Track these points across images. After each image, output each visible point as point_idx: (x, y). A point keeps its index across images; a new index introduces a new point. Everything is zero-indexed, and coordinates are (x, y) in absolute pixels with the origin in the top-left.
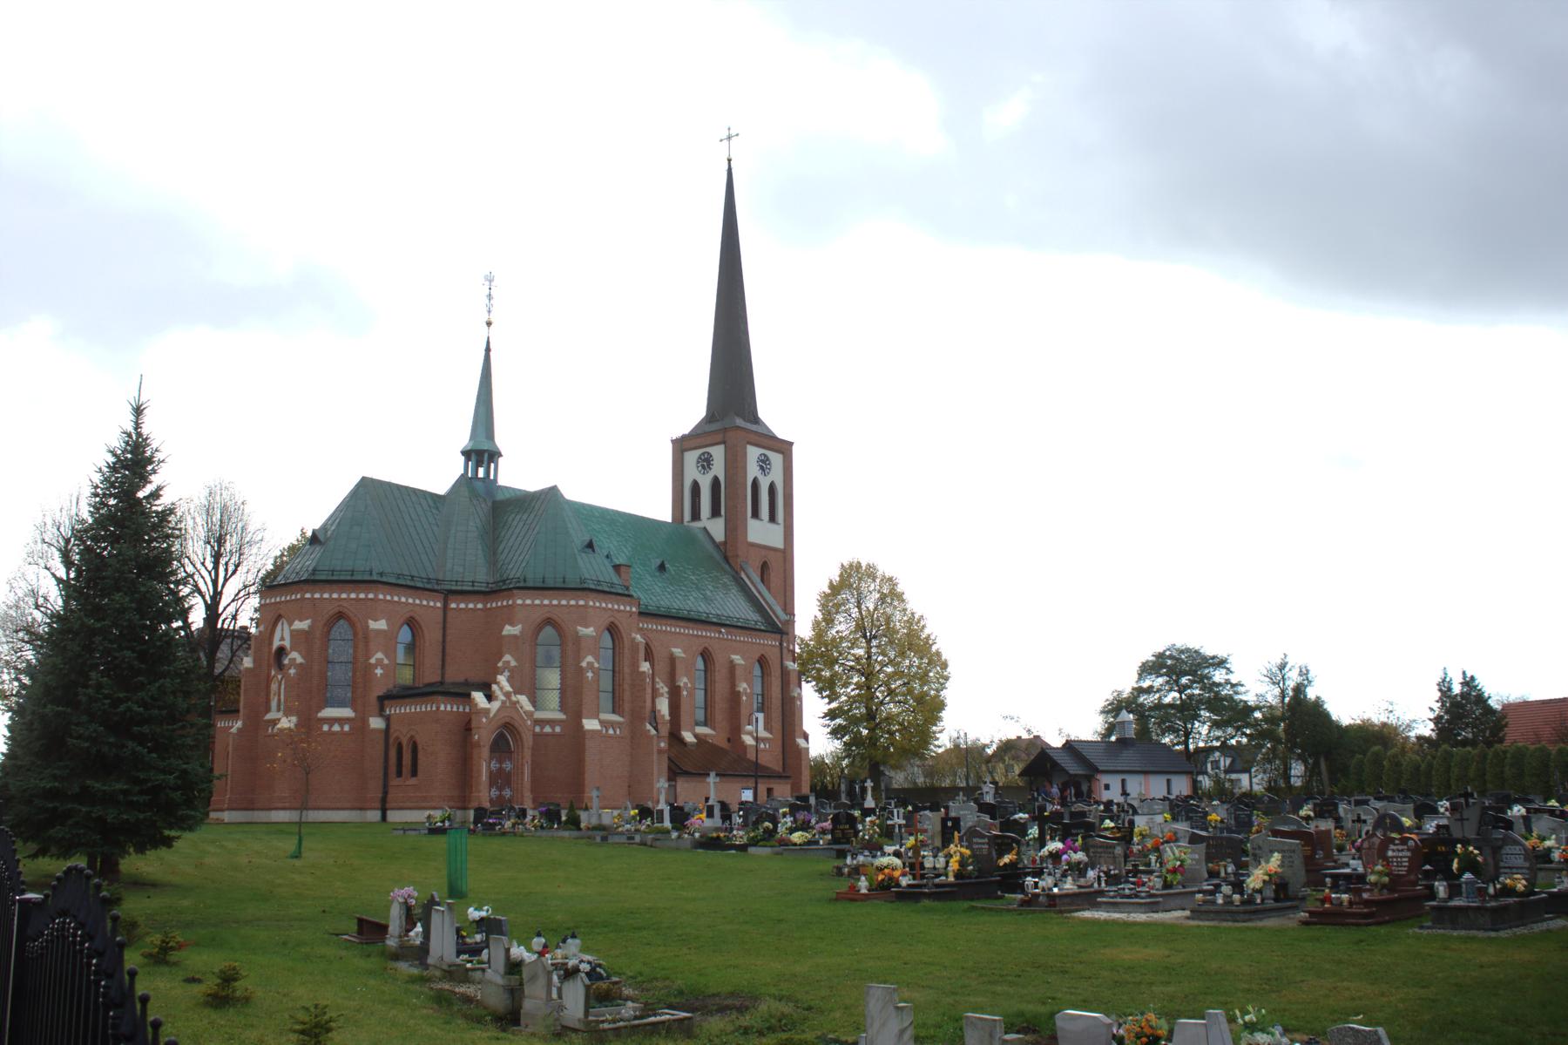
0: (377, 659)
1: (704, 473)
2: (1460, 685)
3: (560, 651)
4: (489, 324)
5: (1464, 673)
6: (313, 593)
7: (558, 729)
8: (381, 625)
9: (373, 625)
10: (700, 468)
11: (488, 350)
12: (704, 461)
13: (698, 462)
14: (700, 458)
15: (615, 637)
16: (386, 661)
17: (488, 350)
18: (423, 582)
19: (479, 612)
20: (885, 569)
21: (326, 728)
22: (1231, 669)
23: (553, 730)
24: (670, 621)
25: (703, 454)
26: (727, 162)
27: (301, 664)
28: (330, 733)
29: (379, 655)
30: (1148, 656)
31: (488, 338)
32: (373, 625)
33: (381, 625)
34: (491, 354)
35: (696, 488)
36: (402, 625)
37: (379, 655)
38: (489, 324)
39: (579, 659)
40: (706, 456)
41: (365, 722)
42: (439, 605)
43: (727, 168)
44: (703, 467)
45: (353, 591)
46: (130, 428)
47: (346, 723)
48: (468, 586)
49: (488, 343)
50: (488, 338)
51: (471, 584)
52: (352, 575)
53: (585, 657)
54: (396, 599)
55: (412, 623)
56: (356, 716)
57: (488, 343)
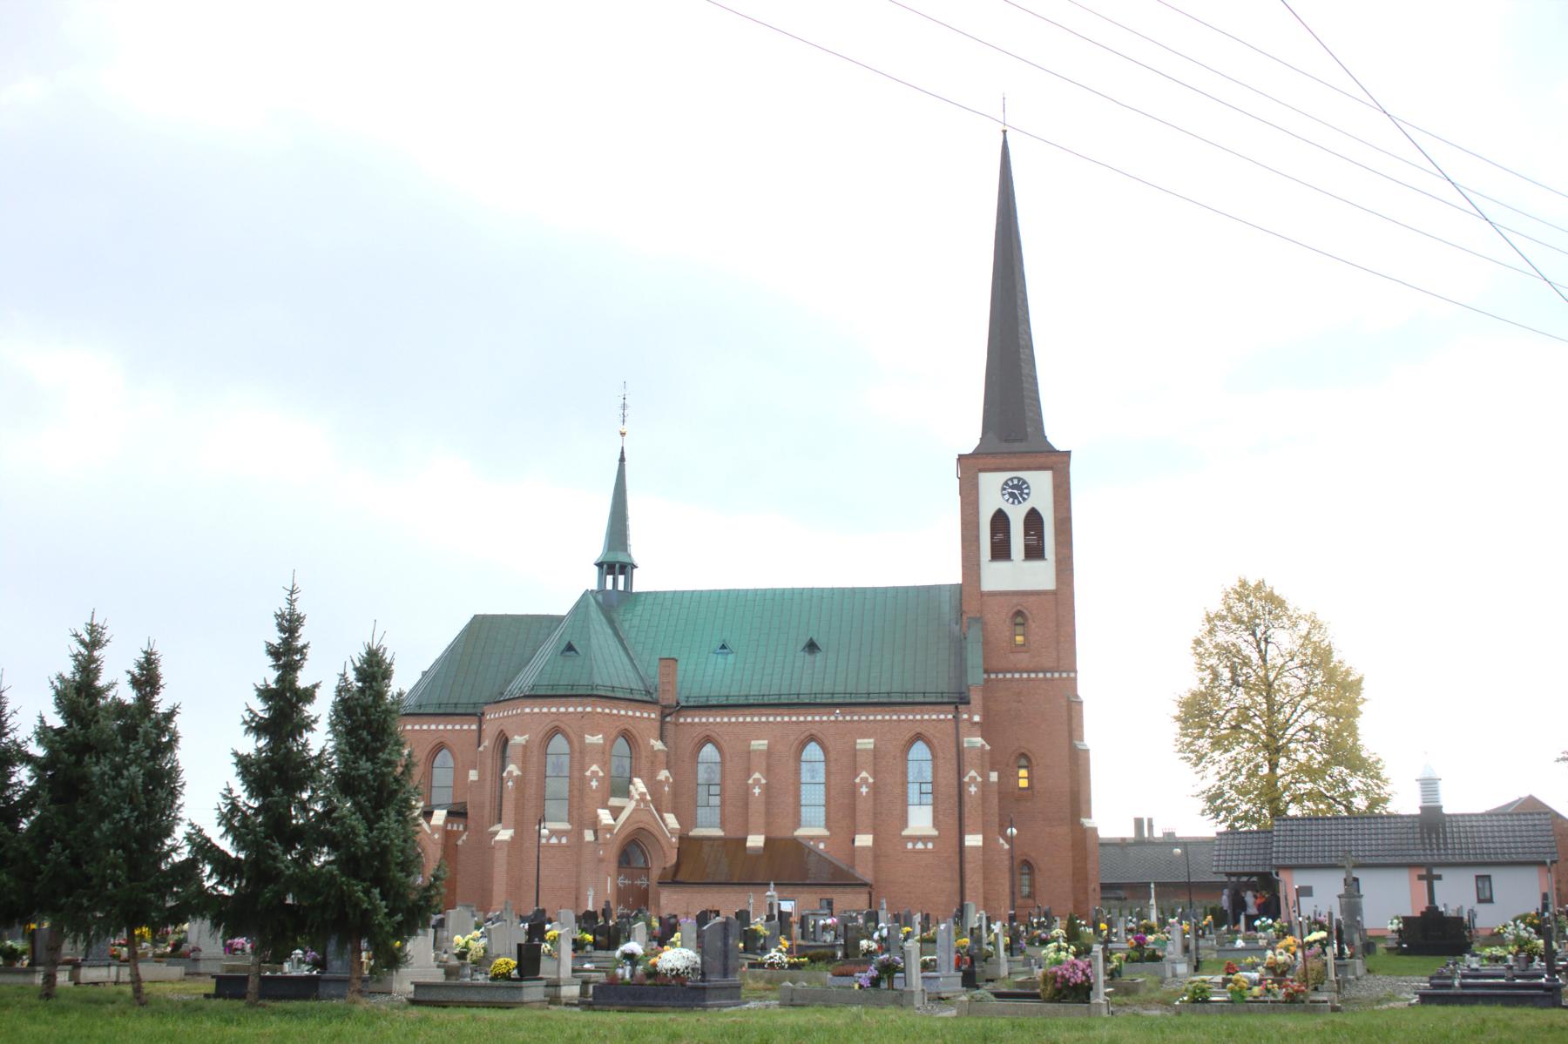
0: (861, 779)
1: (1013, 503)
2: (1178, 725)
3: (931, 766)
4: (623, 434)
5: (1440, 780)
6: (693, 717)
7: (564, 840)
8: (598, 739)
9: (589, 739)
10: (1007, 497)
11: (622, 459)
12: (1013, 487)
13: (1004, 489)
14: (1006, 483)
15: (630, 742)
16: (601, 774)
17: (622, 459)
18: (624, 692)
19: (629, 719)
20: (1198, 628)
21: (910, 846)
22: (306, 643)
23: (560, 841)
24: (764, 710)
25: (1012, 479)
26: (1002, 134)
27: (517, 776)
28: (915, 852)
29: (595, 768)
30: (163, 670)
31: (623, 448)
32: (589, 739)
33: (598, 739)
34: (626, 463)
35: (1000, 521)
36: (616, 738)
37: (595, 768)
38: (623, 434)
39: (583, 769)
40: (1016, 482)
41: (581, 835)
42: (950, 717)
43: (1002, 141)
44: (1012, 495)
45: (818, 714)
46: (285, 606)
47: (930, 841)
48: (884, 697)
49: (622, 452)
50: (623, 448)
51: (570, 687)
52: (832, 698)
53: (969, 772)
54: (638, 714)
55: (627, 735)
56: (939, 834)
57: (622, 452)
